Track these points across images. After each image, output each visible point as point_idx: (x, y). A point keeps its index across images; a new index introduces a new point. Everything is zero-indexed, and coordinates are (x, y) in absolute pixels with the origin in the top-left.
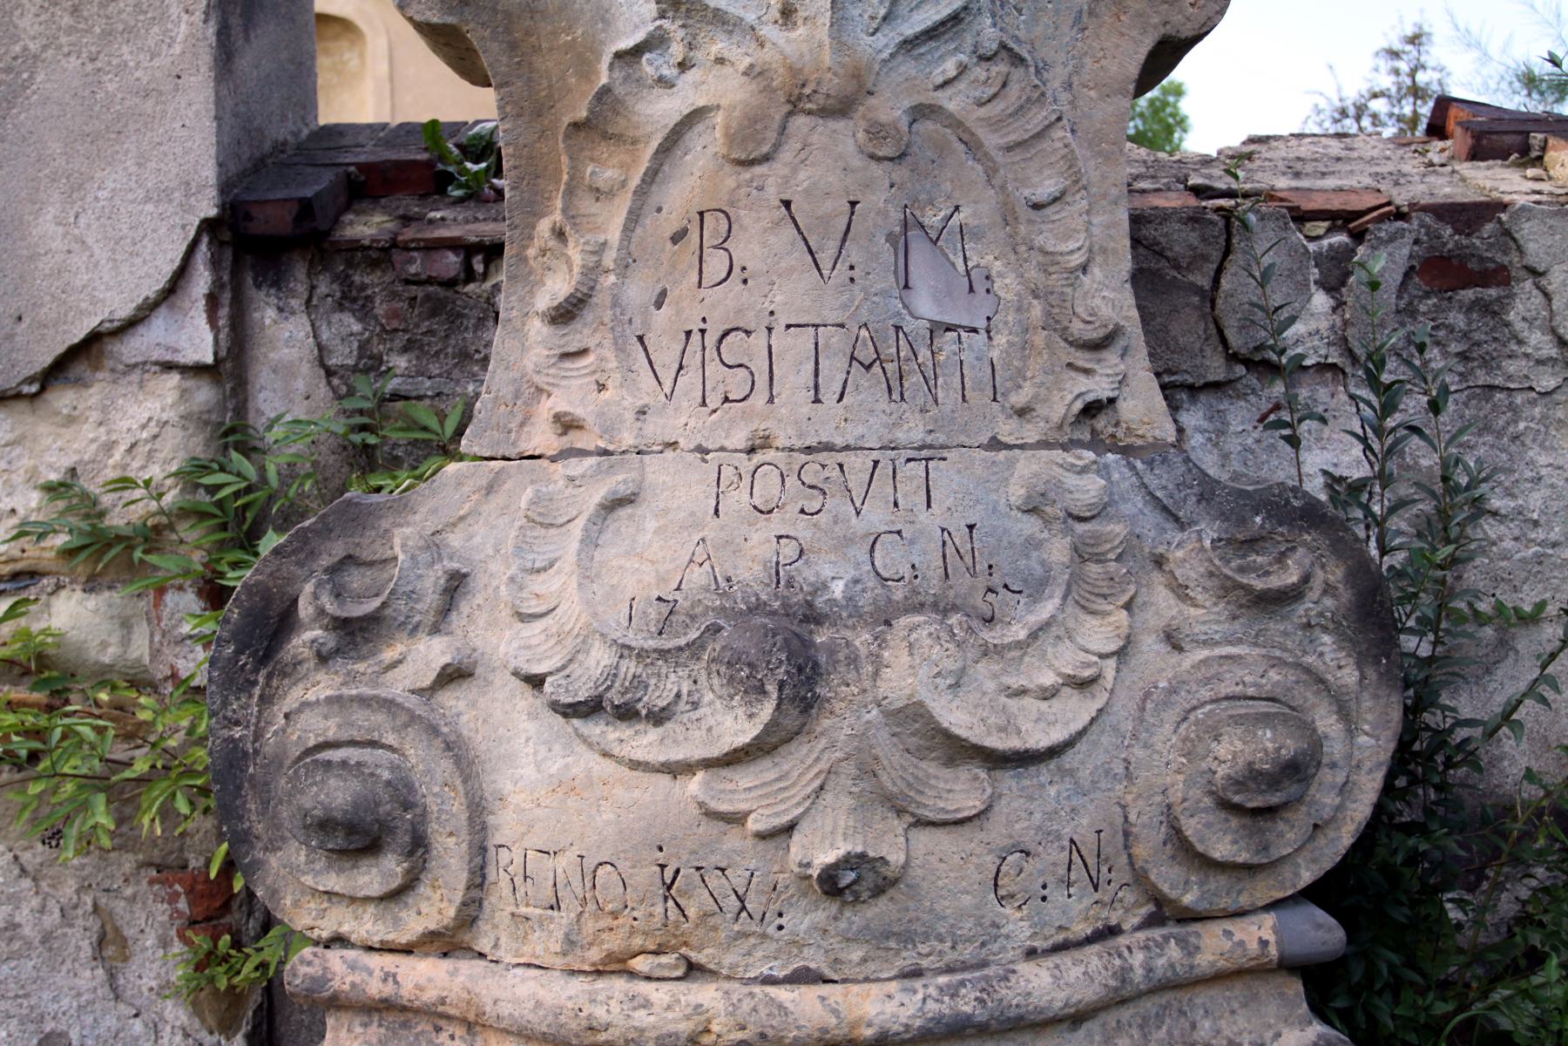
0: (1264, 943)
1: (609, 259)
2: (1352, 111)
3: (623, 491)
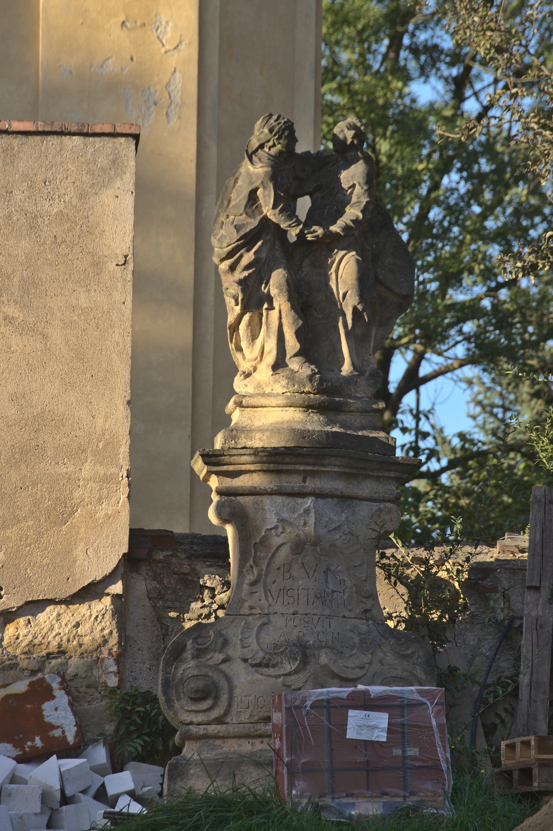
1: (263, 573)
3: (266, 621)
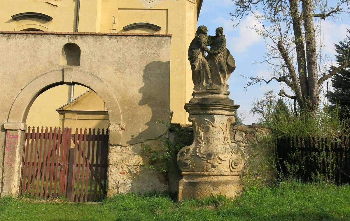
2: (260, 103)
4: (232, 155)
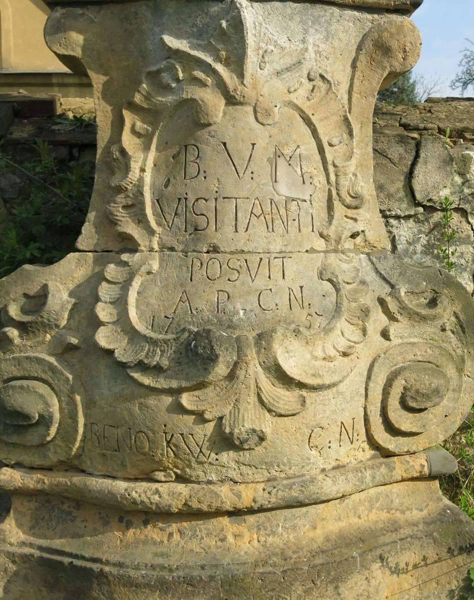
0: (423, 466)
4: (385, 335)
